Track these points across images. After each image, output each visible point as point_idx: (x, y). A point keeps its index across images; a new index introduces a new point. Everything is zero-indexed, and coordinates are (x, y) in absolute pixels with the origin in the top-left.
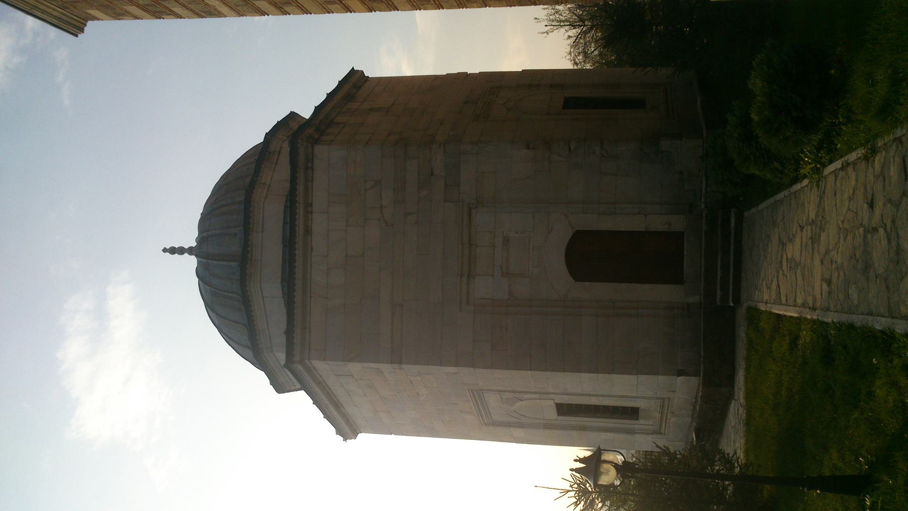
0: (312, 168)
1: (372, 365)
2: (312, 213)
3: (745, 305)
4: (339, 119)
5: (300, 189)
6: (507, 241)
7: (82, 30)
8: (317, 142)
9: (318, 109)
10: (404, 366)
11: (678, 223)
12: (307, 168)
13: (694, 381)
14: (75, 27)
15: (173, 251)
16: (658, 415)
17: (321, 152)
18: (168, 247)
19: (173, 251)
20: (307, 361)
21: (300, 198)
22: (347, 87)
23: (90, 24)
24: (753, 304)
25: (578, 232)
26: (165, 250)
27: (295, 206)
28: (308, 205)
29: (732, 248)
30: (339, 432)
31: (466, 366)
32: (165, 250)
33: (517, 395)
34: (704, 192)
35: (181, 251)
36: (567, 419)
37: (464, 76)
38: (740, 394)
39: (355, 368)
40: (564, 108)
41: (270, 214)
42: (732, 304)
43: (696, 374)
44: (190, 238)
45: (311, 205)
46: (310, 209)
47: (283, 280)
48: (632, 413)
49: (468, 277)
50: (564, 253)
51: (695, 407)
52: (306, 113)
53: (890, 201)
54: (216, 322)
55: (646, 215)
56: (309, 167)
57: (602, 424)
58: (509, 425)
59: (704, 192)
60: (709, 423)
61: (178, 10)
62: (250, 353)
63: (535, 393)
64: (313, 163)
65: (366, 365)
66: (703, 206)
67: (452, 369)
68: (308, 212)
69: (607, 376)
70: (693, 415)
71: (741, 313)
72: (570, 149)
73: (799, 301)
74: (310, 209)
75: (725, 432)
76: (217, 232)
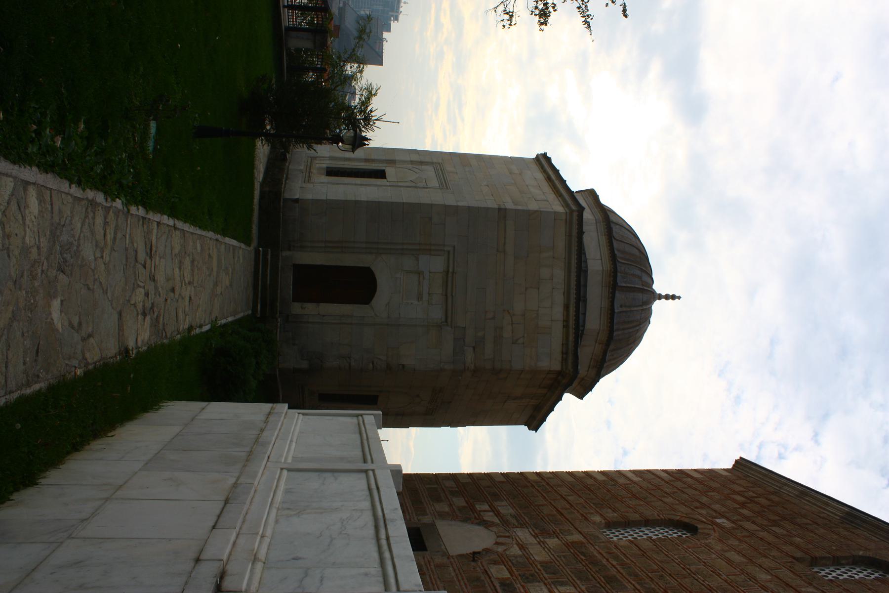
1: (520, 208)
3: (252, 248)
5: (571, 338)
6: (420, 298)
7: (736, 461)
8: (559, 373)
10: (496, 207)
11: (297, 308)
12: (567, 353)
14: (741, 464)
15: (673, 297)
16: (315, 171)
17: (556, 366)
19: (673, 297)
21: (572, 331)
23: (730, 467)
24: (248, 248)
26: (679, 298)
27: (576, 328)
28: (566, 326)
30: (549, 160)
31: (450, 206)
32: (679, 298)
33: (413, 184)
35: (667, 297)
36: (376, 169)
37: (454, 424)
38: (257, 186)
39: (533, 206)
40: (377, 397)
41: (594, 321)
43: (286, 200)
44: (658, 307)
45: (564, 326)
48: (332, 172)
49: (448, 272)
52: (568, 397)
53: (183, 298)
54: (634, 239)
56: (565, 353)
57: (353, 163)
58: (422, 163)
60: (278, 163)
61: (664, 475)
62: (612, 218)
65: (525, 208)
67: (460, 204)
69: (349, 198)
71: (255, 243)
73: (223, 246)
75: (266, 159)
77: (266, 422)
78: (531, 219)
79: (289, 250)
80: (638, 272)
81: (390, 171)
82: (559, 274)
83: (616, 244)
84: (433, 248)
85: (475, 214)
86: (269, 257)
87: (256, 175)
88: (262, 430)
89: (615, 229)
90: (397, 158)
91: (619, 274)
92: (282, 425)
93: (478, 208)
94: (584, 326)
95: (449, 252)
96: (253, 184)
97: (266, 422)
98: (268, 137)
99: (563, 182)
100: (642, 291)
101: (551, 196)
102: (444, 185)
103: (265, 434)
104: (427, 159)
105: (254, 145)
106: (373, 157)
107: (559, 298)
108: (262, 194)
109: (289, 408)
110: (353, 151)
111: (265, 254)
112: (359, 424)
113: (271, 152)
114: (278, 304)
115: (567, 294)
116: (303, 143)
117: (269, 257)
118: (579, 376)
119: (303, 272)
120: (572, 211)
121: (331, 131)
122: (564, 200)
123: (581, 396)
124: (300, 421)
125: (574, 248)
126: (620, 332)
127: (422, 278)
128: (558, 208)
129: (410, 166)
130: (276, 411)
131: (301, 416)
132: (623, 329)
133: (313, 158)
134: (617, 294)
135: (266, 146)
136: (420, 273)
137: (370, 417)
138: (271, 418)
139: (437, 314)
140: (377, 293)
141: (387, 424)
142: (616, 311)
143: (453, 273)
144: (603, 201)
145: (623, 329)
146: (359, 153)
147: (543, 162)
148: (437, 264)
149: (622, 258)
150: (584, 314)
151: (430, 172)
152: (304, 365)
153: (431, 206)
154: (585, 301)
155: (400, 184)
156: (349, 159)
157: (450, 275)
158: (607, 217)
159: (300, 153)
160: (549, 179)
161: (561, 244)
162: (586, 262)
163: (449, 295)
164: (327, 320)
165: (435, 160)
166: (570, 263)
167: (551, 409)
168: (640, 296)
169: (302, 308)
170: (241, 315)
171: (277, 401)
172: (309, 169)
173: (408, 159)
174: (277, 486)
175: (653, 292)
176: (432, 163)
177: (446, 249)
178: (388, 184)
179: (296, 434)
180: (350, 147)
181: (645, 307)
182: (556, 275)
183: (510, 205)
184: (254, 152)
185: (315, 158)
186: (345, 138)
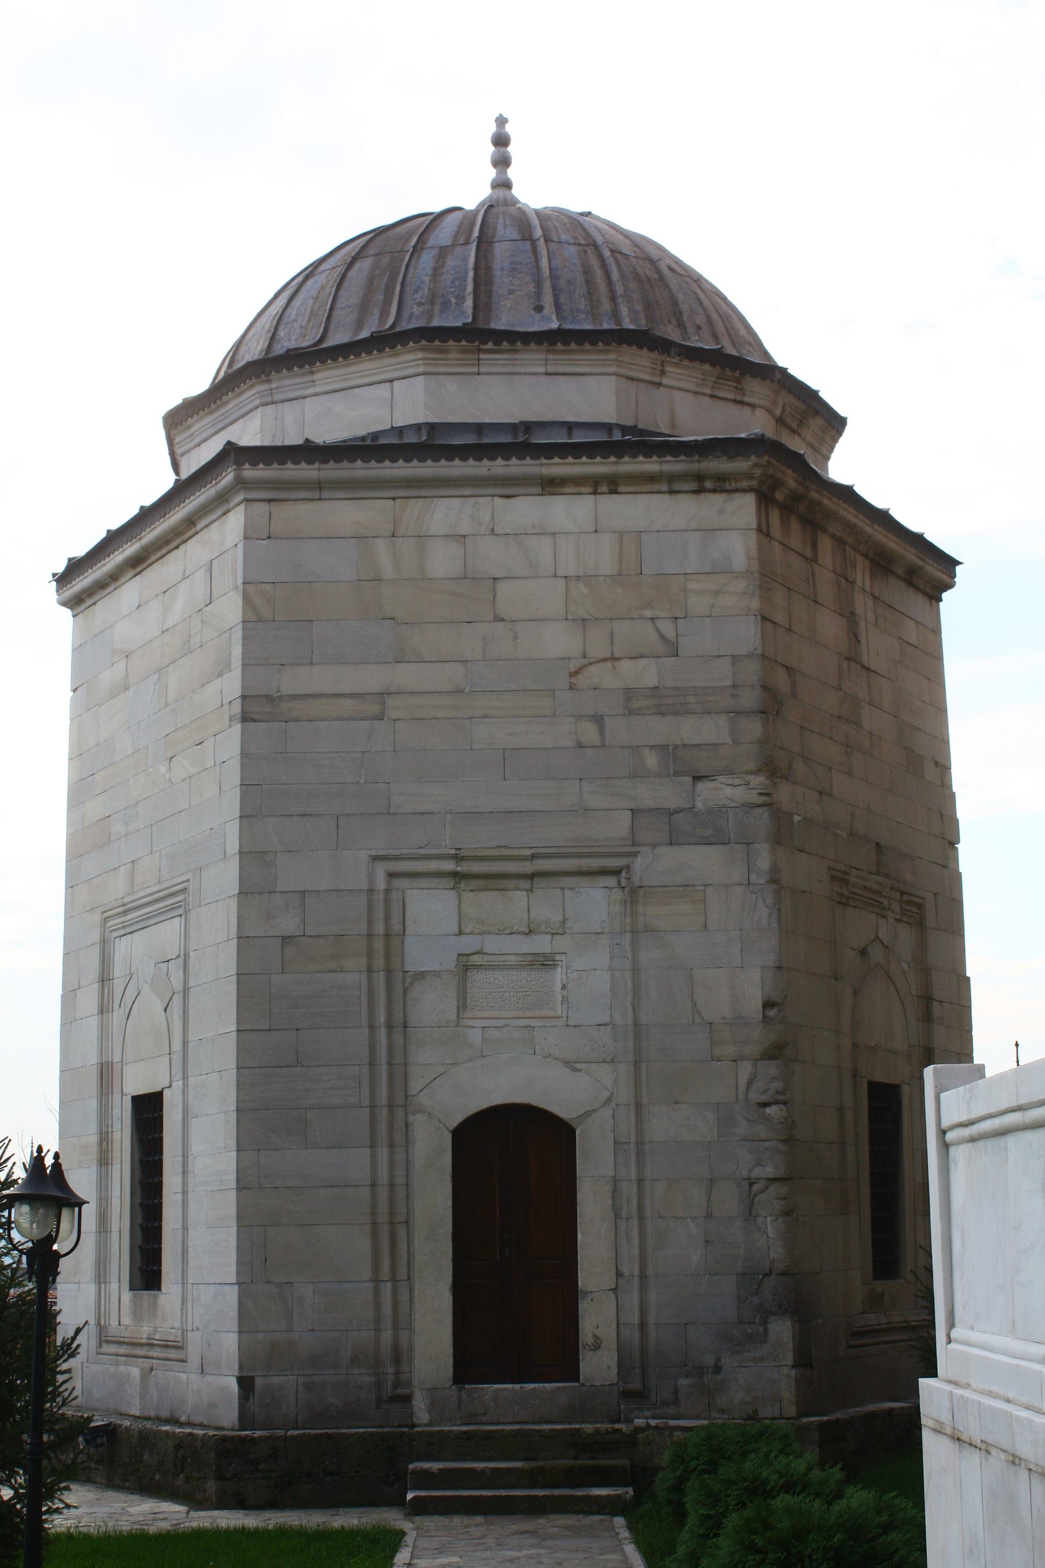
0: (698, 491)
1: (237, 652)
2: (595, 493)
3: (407, 1526)
4: (826, 545)
5: (650, 465)
6: (545, 962)
8: (765, 498)
9: (847, 493)
10: (238, 727)
11: (598, 1366)
12: (700, 478)
13: (228, 1416)
15: (501, 141)
16: (145, 1331)
17: (743, 509)
18: (509, 128)
19: (501, 141)
20: (241, 497)
21: (628, 466)
22: (911, 555)
24: (409, 1539)
25: (572, 1131)
26: (501, 121)
27: (620, 452)
28: (613, 485)
29: (541, 1493)
30: (75, 567)
32: (501, 121)
34: (673, 1423)
35: (502, 162)
37: (947, 836)
39: (230, 609)
41: (589, 394)
42: (410, 1496)
43: (245, 1419)
44: (535, 191)
45: (613, 492)
46: (604, 488)
47: (432, 428)
48: (147, 1273)
49: (454, 874)
50: (518, 1100)
51: (167, 1421)
52: (842, 466)
54: (319, 279)
55: (614, 1290)
56: (701, 484)
57: (116, 1202)
58: (105, 979)
59: (673, 1423)
60: (124, 1455)
62: (254, 351)
63: (185, 1043)
64: (714, 491)
65: (238, 635)
66: (639, 1422)
67: (233, 845)
68: (599, 485)
69: (232, 1211)
70: (147, 1418)
71: (392, 1518)
72: (765, 1105)
74: (604, 488)
75: (111, 1494)
76: (544, 263)
77: (985, 1448)
78: (274, 617)
79: (407, 1399)
80: (427, 259)
81: (138, 1081)
82: (445, 513)
83: (338, 337)
84: (380, 928)
85: (262, 800)
86: (435, 1466)
87: (165, 1525)
88: (1015, 1460)
89: (290, 340)
90: (93, 1059)
91: (436, 323)
92: (990, 1394)
93: (247, 786)
94: (608, 427)
95: (392, 875)
96: (198, 1534)
97: (985, 1448)
98: (39, 1493)
99: (146, 516)
100: (485, 243)
101: (194, 552)
102: (174, 901)
103: (1025, 1450)
104: (92, 960)
105: (68, 1537)
106: (94, 1139)
107: (525, 510)
108: (223, 1503)
109: (932, 1372)
110: (80, 1203)
111: (426, 1480)
112: (972, 1140)
113: (87, 1480)
114: (589, 1428)
115: (508, 487)
116: (55, 1372)
117: (435, 1466)
118: (770, 433)
119: (477, 1355)
120: (240, 483)
121: (13, 1282)
122: (206, 509)
123: (835, 424)
124: (975, 1336)
125: (361, 470)
126: (624, 310)
127: (476, 959)
128: (229, 529)
129: (117, 1016)
130: (945, 1417)
131: (954, 1334)
132: (613, 299)
133: (103, 1337)
134: (501, 323)
135: (70, 1498)
136: (465, 966)
137: (946, 1103)
138: (973, 1431)
139: (595, 903)
140: (534, 1102)
141: (960, 1049)
142: (555, 325)
143: (458, 858)
144: (200, 383)
145: (613, 299)
146: (81, 1181)
147: (84, 581)
148: (432, 914)
149: (384, 314)
150: (570, 427)
151: (134, 951)
152: (782, 1330)
153: (242, 939)
154: (528, 427)
155: (177, 1046)
156: (103, 1218)
157: (463, 868)
158: (254, 370)
159: (93, 1382)
160: (138, 563)
161: (346, 514)
162: (400, 431)
163: (528, 868)
164: (642, 1259)
165: (95, 935)
166: (409, 483)
167: (883, 518)
168: (501, 251)
169: (596, 1347)
170: (631, 1550)
171: (915, 1413)
172: (136, 1347)
173: (94, 1023)
174: (1005, 1353)
175: (490, 207)
176: (105, 943)
177: (381, 884)
178: (178, 1084)
179: (1019, 1346)
180: (65, 1213)
181: (538, 233)
182: (452, 524)
183: (232, 685)
184: (88, 1537)
185: (101, 1328)
186: (37, 1233)
